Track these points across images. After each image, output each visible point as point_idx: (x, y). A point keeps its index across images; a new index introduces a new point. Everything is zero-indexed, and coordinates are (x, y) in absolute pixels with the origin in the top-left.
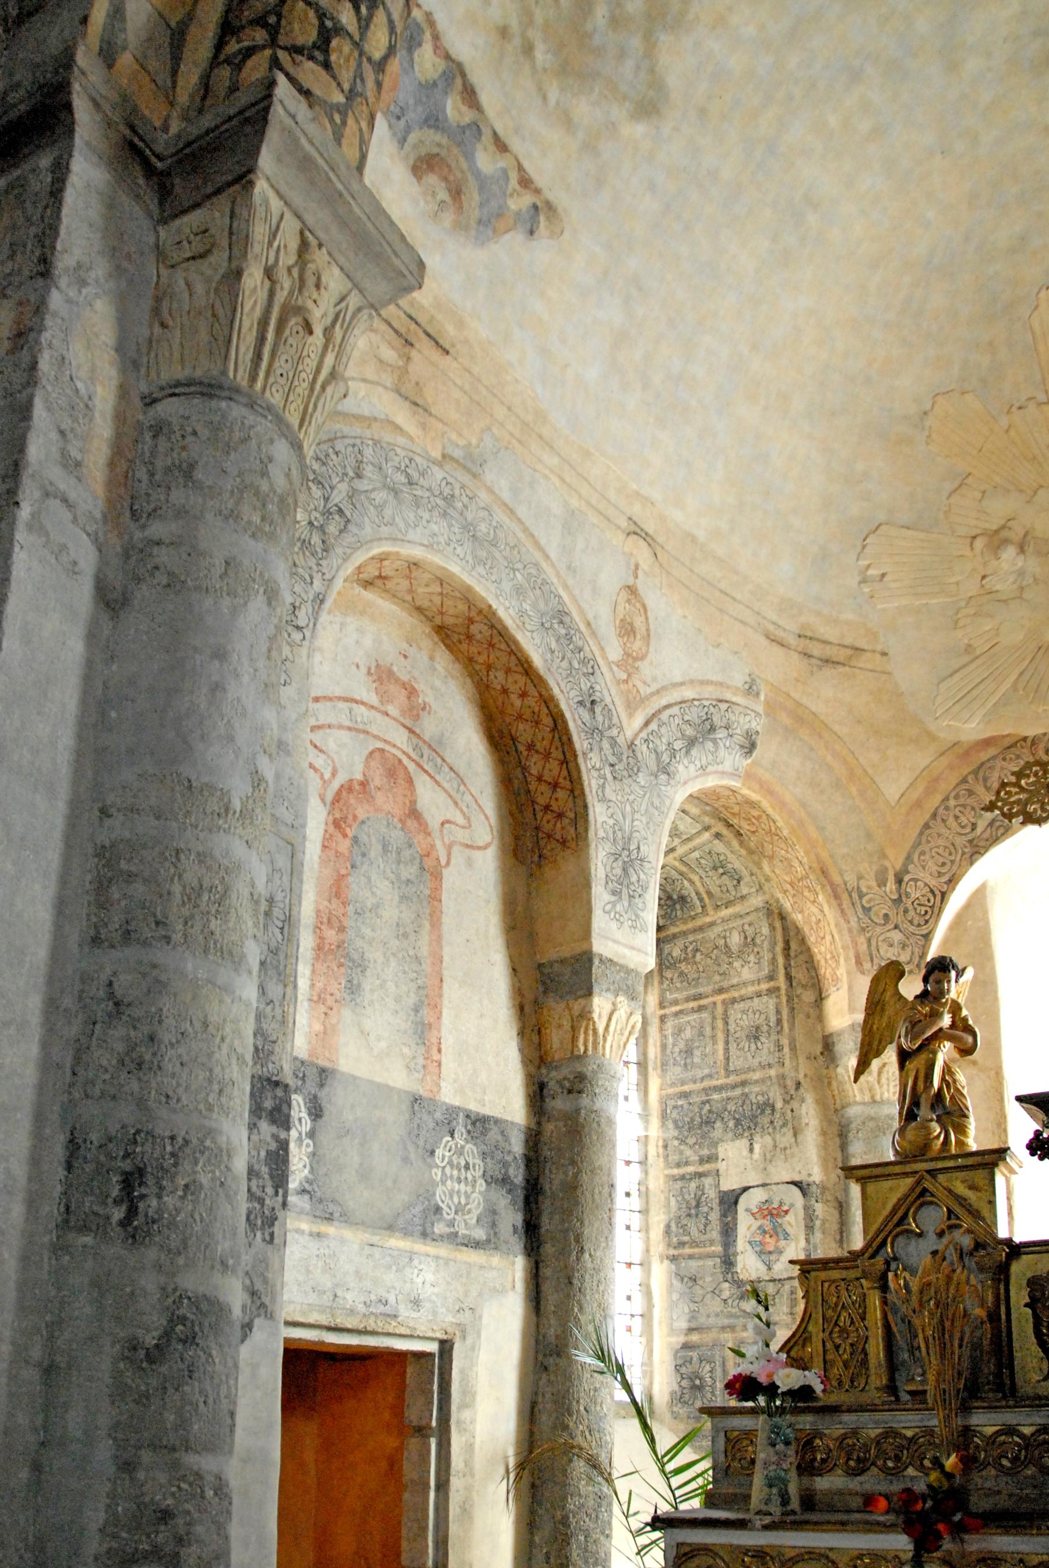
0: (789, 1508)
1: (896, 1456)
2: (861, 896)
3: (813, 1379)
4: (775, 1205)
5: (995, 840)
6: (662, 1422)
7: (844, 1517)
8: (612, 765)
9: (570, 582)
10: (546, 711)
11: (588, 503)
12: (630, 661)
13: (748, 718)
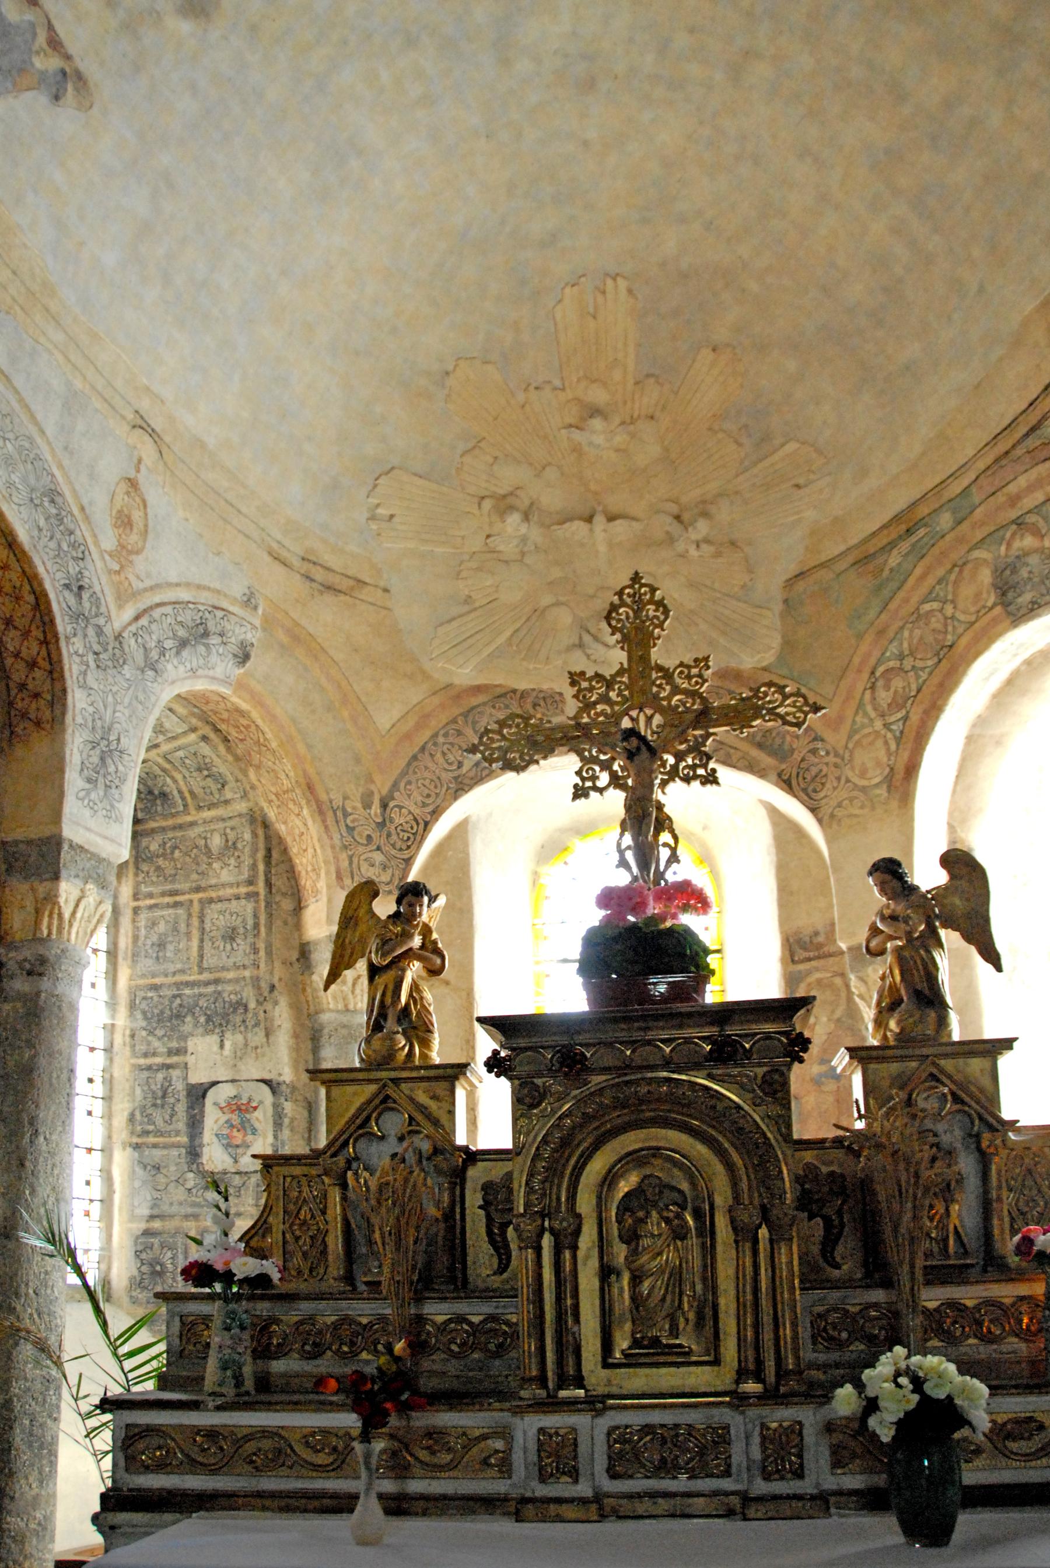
0: (243, 1389)
1: (351, 1341)
2: (346, 815)
3: (271, 1268)
4: (244, 1101)
5: (479, 780)
6: (120, 1306)
7: (301, 1398)
8: (96, 653)
9: (66, 462)
10: (28, 587)
11: (93, 388)
12: (124, 553)
13: (243, 629)
